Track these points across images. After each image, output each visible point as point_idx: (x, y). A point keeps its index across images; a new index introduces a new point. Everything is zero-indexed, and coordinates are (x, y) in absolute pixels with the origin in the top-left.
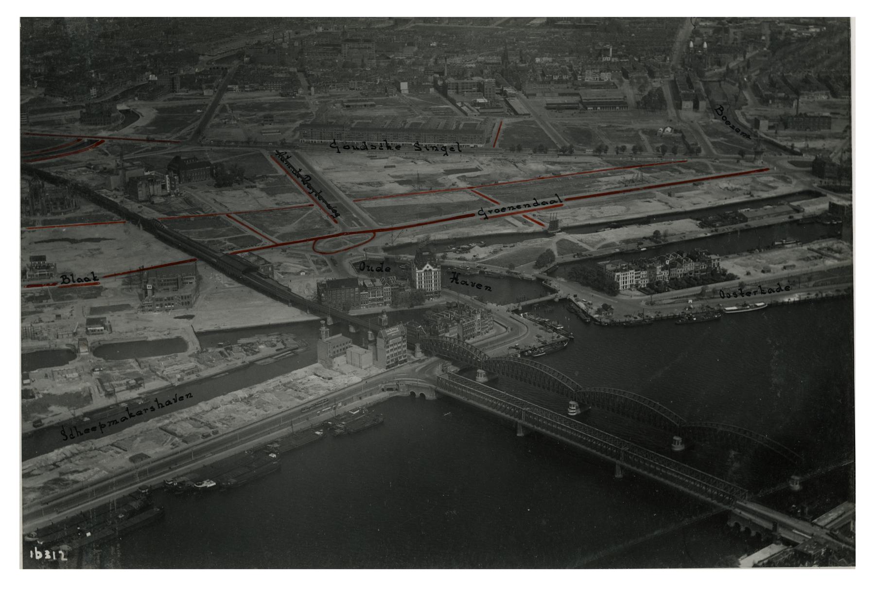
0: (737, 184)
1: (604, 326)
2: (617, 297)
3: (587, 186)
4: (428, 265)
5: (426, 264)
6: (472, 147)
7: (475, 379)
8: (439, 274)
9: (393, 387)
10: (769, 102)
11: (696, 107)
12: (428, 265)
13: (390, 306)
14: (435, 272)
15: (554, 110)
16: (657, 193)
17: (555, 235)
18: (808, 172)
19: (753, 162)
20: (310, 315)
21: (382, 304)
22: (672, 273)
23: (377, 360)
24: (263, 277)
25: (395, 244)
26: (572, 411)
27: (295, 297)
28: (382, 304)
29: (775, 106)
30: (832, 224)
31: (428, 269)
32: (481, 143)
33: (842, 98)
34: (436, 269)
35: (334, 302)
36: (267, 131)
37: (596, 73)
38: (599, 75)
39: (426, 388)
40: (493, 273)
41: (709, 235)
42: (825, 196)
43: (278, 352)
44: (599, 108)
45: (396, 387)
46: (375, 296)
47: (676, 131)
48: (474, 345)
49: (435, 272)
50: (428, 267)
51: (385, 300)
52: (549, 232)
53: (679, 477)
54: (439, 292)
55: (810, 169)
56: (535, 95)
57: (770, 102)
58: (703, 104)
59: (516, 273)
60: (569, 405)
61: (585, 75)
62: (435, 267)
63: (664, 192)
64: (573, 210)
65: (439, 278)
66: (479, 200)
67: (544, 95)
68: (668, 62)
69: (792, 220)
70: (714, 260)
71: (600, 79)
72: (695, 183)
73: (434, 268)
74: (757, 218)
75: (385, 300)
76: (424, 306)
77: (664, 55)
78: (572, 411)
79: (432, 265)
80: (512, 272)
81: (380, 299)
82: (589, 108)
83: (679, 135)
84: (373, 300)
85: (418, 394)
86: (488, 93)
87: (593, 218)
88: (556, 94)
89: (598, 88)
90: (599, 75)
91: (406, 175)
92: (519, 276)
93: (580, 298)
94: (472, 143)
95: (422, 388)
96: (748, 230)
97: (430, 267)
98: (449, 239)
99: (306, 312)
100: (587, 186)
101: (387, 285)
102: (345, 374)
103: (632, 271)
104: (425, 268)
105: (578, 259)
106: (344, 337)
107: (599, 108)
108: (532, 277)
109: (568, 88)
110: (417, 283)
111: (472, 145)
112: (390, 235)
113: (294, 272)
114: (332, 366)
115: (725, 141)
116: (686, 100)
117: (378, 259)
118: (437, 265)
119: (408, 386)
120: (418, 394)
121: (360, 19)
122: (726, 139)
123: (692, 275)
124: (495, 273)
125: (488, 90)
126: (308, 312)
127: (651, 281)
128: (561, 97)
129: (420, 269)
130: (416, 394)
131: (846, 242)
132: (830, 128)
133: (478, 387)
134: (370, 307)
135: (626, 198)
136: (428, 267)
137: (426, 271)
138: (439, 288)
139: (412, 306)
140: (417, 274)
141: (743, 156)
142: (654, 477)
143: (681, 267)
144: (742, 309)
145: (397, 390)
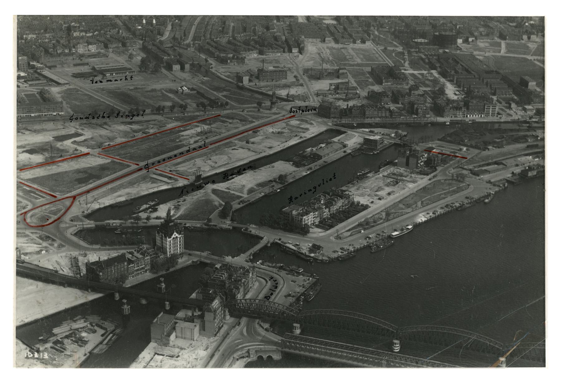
2: (309, 235)
3: (178, 140)
4: (175, 233)
5: (173, 232)
7: (292, 332)
10: (227, 61)
11: (183, 68)
12: (175, 233)
13: (149, 272)
14: (180, 238)
16: (236, 141)
19: (269, 110)
20: (92, 293)
21: (144, 272)
22: (331, 210)
25: (89, 211)
26: (397, 348)
28: (144, 272)
29: (233, 64)
30: (374, 154)
31: (175, 237)
32: (62, 111)
33: (266, 55)
34: (181, 236)
38: (88, 48)
41: (308, 172)
43: (104, 338)
44: (114, 74)
46: (139, 266)
47: (192, 89)
49: (180, 238)
50: (175, 235)
53: (338, 353)
56: (56, 66)
57: (229, 61)
58: (187, 66)
60: (393, 344)
61: (77, 48)
62: (180, 234)
63: (240, 140)
66: (111, 162)
69: (346, 154)
71: (89, 50)
72: (254, 130)
73: (179, 235)
74: (326, 155)
77: (117, 29)
78: (397, 348)
79: (178, 233)
80: (211, 225)
81: (142, 268)
83: (195, 92)
84: (138, 270)
86: (22, 68)
88: (72, 65)
89: (94, 58)
90: (88, 48)
93: (285, 241)
94: (54, 112)
95: (270, 351)
97: (177, 235)
98: (127, 200)
99: (88, 291)
101: (147, 256)
102: (185, 349)
103: (311, 214)
104: (173, 236)
105: (243, 205)
110: (168, 249)
112: (78, 203)
114: (169, 343)
116: (175, 64)
120: (265, 357)
121: (105, 17)
123: (341, 210)
124: (196, 227)
125: (22, 65)
126: (90, 291)
129: (170, 237)
130: (264, 357)
131: (402, 168)
132: (286, 79)
133: (296, 338)
134: (136, 276)
135: (219, 148)
136: (175, 235)
137: (174, 238)
138: (183, 250)
139: (168, 270)
140: (168, 242)
143: (335, 205)
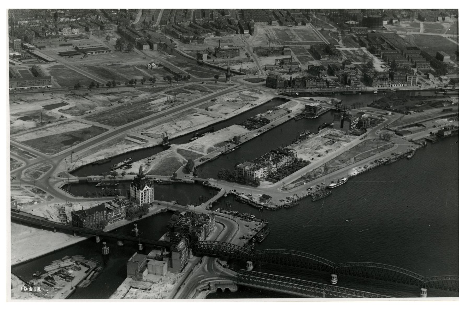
0: (233, 98)
1: (274, 210)
3: (148, 108)
4: (146, 186)
6: (44, 88)
7: (246, 268)
8: (152, 191)
9: (206, 288)
10: (189, 42)
11: (151, 48)
12: (146, 186)
13: (125, 219)
14: (151, 190)
15: (67, 57)
17: (169, 147)
18: (263, 85)
19: (225, 82)
20: (77, 237)
21: (120, 219)
23: (172, 267)
24: (16, 212)
25: (74, 168)
26: (335, 281)
27: (57, 225)
28: (120, 219)
29: (194, 44)
32: (50, 85)
33: (222, 36)
35: (91, 224)
36: (158, 120)
37: (70, 30)
39: (230, 284)
40: (162, 181)
42: (289, 100)
43: (87, 274)
45: (208, 287)
46: (116, 214)
47: (160, 65)
48: (218, 240)
49: (151, 190)
50: (146, 187)
51: (122, 216)
52: (163, 145)
54: (153, 203)
55: (265, 82)
56: (45, 47)
58: (155, 46)
59: (180, 180)
60: (331, 278)
62: (150, 187)
64: (161, 125)
65: (152, 194)
67: (51, 47)
68: (99, 19)
69: (290, 118)
70: (295, 153)
71: (72, 33)
74: (274, 120)
75: (122, 216)
76: (149, 214)
77: (96, 15)
78: (335, 281)
80: (177, 179)
81: (119, 216)
82: (88, 54)
84: (115, 217)
85: (223, 289)
86: (17, 48)
87: (178, 131)
88: (58, 45)
89: (77, 39)
91: (22, 113)
92: (182, 181)
94: (44, 85)
96: (274, 128)
97: (148, 188)
99: (73, 235)
100: (148, 108)
101: (123, 205)
102: (156, 283)
104: (145, 189)
105: (203, 162)
106: (138, 254)
107: (94, 53)
108: (192, 181)
109: (60, 40)
110: (140, 200)
111: (44, 87)
113: (27, 202)
114: (142, 278)
115: (191, 69)
116: (145, 44)
117: (75, 182)
118: (151, 185)
119: (216, 285)
120: (223, 289)
122: (191, 68)
123: (286, 165)
124: (164, 181)
125: (17, 46)
126: (75, 235)
127: (269, 173)
128: (61, 47)
130: (222, 289)
131: (338, 129)
133: (250, 273)
134: (113, 222)
136: (146, 187)
137: (145, 190)
140: (140, 194)
141: (217, 79)
142: (257, 286)
143: (282, 161)
144: (338, 185)
145: (208, 289)
